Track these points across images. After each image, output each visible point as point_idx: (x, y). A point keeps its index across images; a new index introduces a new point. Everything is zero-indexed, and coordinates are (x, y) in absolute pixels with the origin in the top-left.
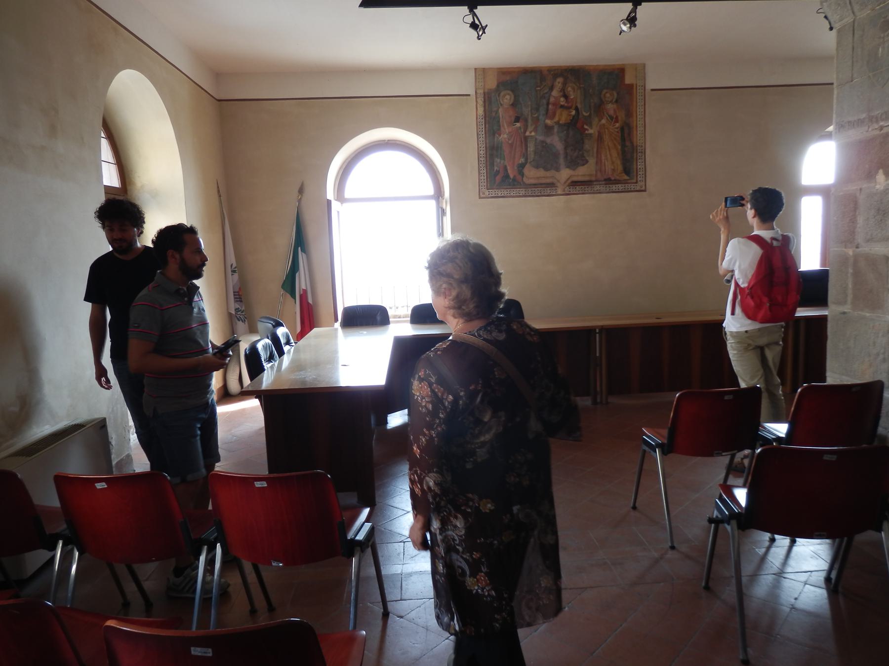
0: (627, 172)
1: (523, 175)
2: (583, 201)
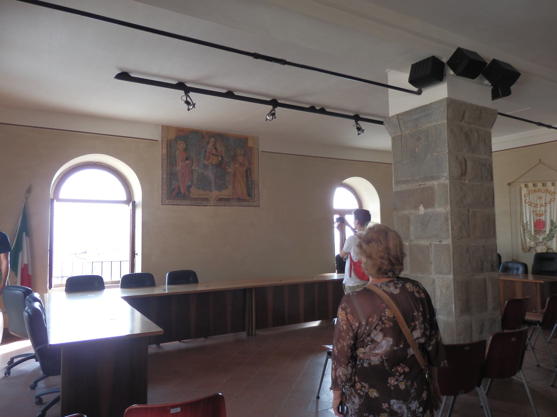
0: (248, 195)
1: (190, 192)
2: (225, 210)
